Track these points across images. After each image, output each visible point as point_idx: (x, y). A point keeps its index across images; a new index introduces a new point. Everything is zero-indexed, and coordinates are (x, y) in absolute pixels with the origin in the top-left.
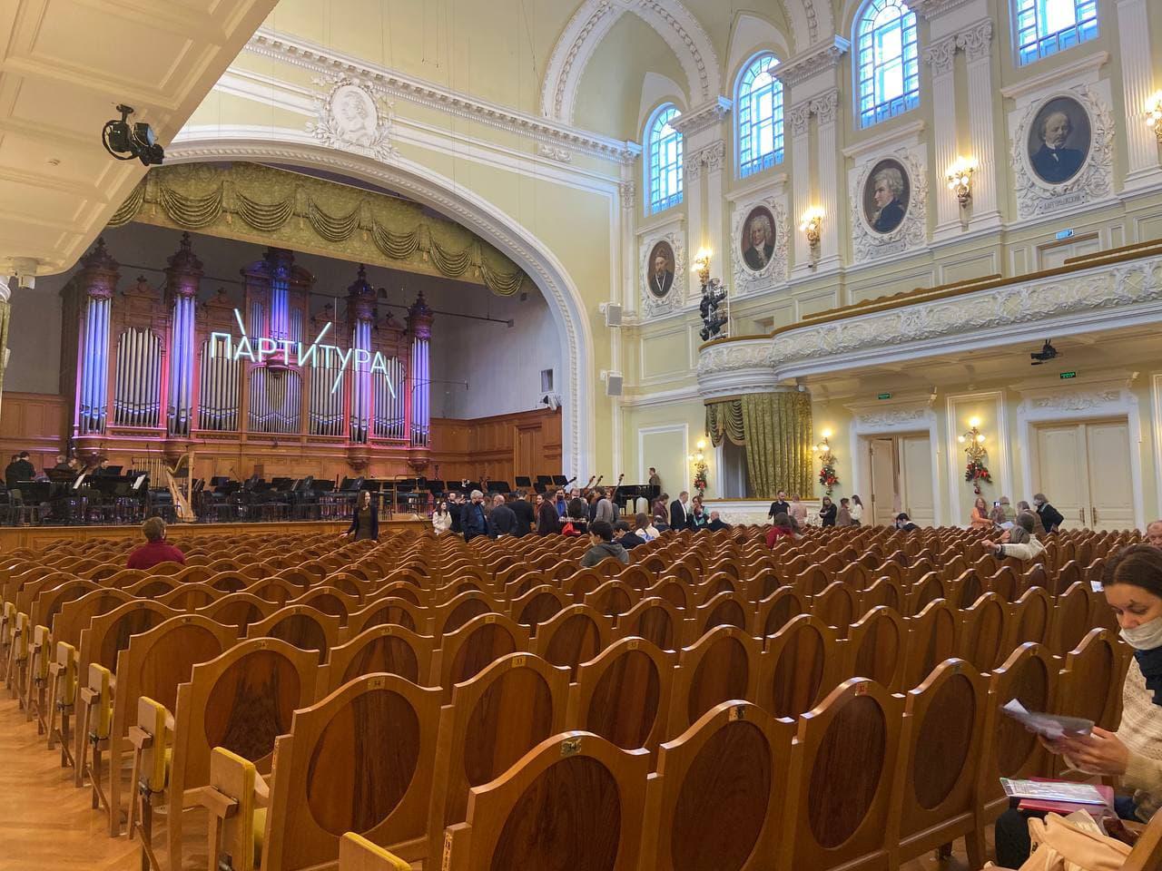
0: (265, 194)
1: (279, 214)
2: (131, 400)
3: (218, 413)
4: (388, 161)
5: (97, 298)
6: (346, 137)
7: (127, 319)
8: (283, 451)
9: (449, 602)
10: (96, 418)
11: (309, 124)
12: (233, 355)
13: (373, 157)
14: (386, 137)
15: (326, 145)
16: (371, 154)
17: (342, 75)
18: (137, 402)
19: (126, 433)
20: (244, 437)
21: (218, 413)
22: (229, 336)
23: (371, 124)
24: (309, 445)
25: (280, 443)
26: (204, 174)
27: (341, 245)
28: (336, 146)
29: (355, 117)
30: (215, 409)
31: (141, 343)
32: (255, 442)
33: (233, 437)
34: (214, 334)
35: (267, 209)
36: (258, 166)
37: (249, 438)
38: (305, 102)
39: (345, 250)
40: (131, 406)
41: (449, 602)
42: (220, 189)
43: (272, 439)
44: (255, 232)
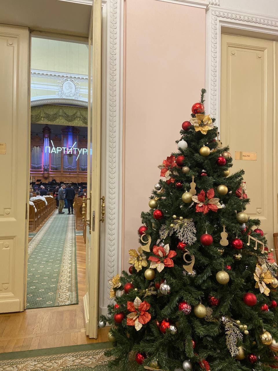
0: (51, 112)
1: (55, 117)
2: (35, 164)
3: (56, 166)
4: (79, 99)
5: (46, 138)
6: (66, 95)
7: (34, 144)
8: (72, 175)
9: (71, 209)
10: (46, 168)
11: (57, 93)
12: (51, 152)
13: (74, 99)
14: (78, 93)
15: (61, 98)
16: (73, 98)
17: (65, 79)
18: (37, 164)
19: (34, 171)
20: (62, 172)
21: (56, 166)
22: (50, 147)
23: (73, 90)
24: (64, 173)
25: (71, 173)
26: (36, 109)
27: (73, 122)
28: (64, 98)
29: (69, 89)
30: (55, 165)
31: (37, 149)
32: (65, 173)
33: (59, 172)
34: (58, 148)
35: (52, 115)
36: (50, 105)
37: (64, 172)
38: (56, 88)
39: (73, 123)
40: (35, 165)
41: (71, 209)
42: (40, 112)
43: (69, 172)
44: (49, 121)
